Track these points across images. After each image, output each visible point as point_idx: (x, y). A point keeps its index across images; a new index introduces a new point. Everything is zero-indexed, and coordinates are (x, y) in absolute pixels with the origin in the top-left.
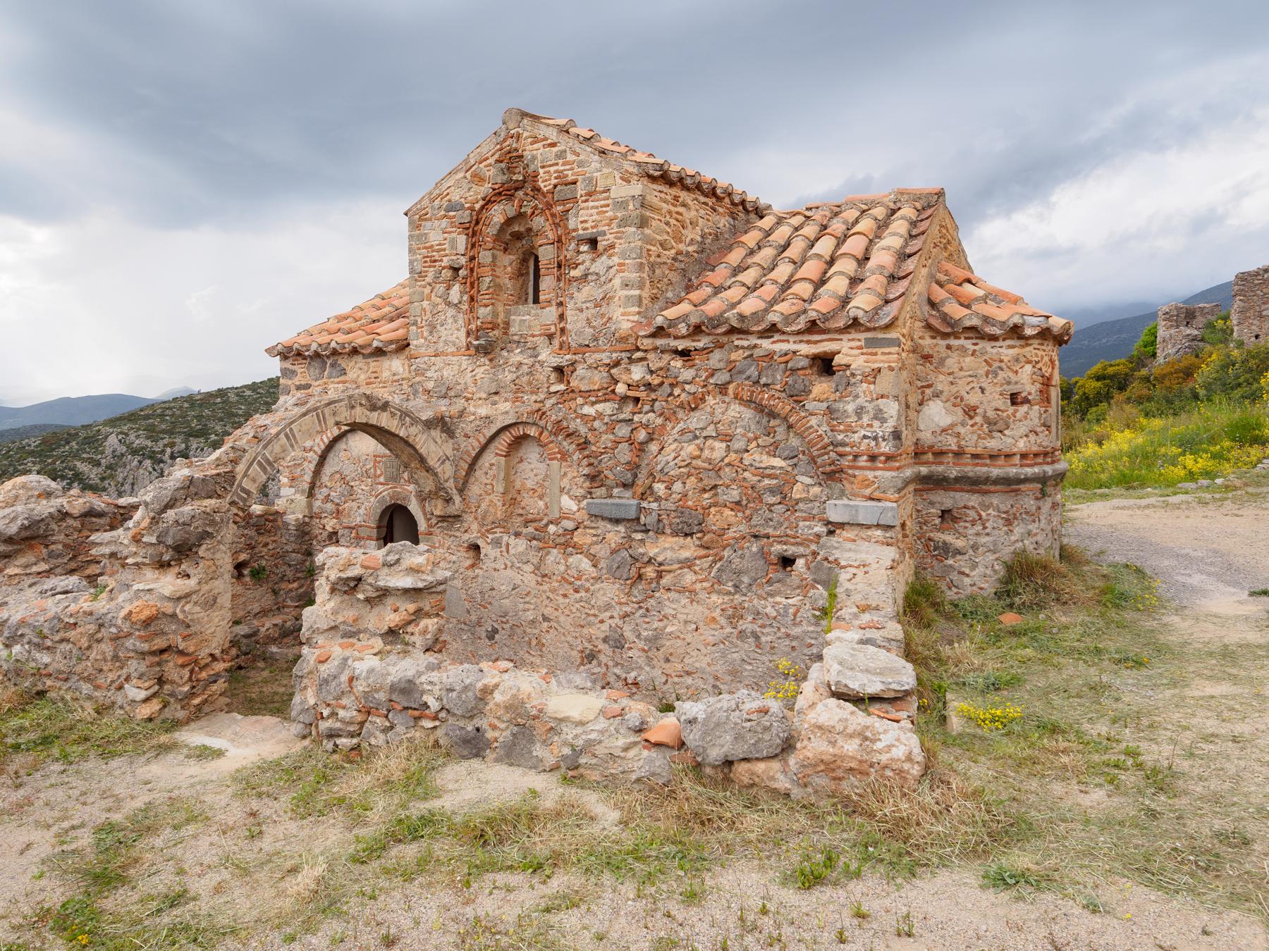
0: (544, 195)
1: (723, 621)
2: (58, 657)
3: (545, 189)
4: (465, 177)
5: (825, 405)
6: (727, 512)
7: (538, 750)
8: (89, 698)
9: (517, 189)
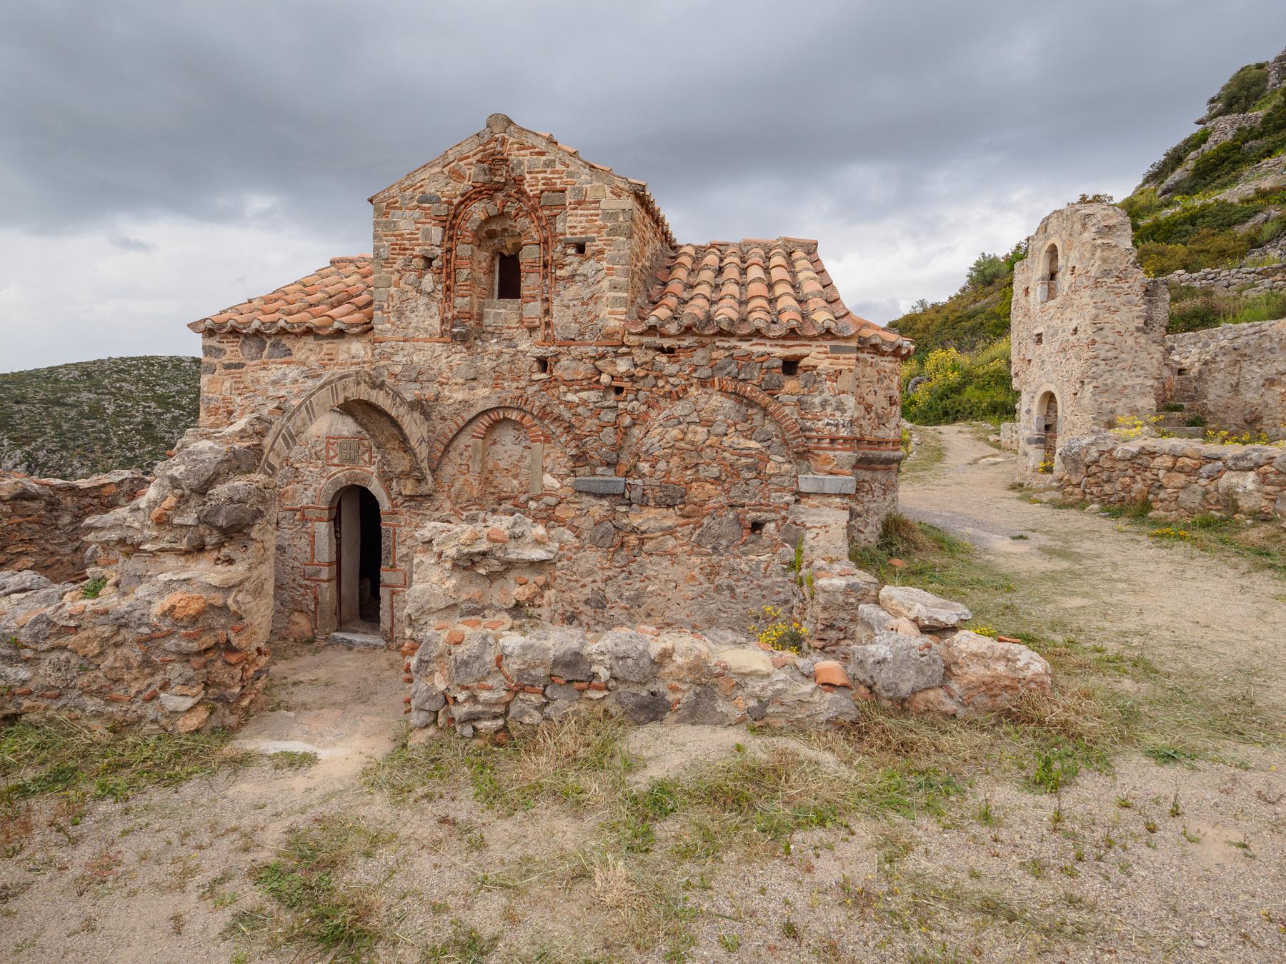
0: (529, 198)
1: (702, 578)
2: (44, 668)
3: (531, 194)
4: (442, 172)
5: (796, 398)
6: (708, 486)
7: (722, 706)
8: (98, 715)
9: (496, 190)
